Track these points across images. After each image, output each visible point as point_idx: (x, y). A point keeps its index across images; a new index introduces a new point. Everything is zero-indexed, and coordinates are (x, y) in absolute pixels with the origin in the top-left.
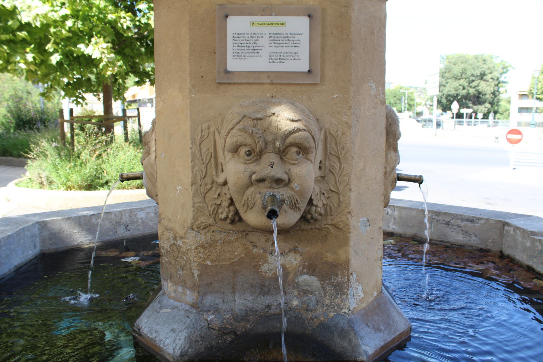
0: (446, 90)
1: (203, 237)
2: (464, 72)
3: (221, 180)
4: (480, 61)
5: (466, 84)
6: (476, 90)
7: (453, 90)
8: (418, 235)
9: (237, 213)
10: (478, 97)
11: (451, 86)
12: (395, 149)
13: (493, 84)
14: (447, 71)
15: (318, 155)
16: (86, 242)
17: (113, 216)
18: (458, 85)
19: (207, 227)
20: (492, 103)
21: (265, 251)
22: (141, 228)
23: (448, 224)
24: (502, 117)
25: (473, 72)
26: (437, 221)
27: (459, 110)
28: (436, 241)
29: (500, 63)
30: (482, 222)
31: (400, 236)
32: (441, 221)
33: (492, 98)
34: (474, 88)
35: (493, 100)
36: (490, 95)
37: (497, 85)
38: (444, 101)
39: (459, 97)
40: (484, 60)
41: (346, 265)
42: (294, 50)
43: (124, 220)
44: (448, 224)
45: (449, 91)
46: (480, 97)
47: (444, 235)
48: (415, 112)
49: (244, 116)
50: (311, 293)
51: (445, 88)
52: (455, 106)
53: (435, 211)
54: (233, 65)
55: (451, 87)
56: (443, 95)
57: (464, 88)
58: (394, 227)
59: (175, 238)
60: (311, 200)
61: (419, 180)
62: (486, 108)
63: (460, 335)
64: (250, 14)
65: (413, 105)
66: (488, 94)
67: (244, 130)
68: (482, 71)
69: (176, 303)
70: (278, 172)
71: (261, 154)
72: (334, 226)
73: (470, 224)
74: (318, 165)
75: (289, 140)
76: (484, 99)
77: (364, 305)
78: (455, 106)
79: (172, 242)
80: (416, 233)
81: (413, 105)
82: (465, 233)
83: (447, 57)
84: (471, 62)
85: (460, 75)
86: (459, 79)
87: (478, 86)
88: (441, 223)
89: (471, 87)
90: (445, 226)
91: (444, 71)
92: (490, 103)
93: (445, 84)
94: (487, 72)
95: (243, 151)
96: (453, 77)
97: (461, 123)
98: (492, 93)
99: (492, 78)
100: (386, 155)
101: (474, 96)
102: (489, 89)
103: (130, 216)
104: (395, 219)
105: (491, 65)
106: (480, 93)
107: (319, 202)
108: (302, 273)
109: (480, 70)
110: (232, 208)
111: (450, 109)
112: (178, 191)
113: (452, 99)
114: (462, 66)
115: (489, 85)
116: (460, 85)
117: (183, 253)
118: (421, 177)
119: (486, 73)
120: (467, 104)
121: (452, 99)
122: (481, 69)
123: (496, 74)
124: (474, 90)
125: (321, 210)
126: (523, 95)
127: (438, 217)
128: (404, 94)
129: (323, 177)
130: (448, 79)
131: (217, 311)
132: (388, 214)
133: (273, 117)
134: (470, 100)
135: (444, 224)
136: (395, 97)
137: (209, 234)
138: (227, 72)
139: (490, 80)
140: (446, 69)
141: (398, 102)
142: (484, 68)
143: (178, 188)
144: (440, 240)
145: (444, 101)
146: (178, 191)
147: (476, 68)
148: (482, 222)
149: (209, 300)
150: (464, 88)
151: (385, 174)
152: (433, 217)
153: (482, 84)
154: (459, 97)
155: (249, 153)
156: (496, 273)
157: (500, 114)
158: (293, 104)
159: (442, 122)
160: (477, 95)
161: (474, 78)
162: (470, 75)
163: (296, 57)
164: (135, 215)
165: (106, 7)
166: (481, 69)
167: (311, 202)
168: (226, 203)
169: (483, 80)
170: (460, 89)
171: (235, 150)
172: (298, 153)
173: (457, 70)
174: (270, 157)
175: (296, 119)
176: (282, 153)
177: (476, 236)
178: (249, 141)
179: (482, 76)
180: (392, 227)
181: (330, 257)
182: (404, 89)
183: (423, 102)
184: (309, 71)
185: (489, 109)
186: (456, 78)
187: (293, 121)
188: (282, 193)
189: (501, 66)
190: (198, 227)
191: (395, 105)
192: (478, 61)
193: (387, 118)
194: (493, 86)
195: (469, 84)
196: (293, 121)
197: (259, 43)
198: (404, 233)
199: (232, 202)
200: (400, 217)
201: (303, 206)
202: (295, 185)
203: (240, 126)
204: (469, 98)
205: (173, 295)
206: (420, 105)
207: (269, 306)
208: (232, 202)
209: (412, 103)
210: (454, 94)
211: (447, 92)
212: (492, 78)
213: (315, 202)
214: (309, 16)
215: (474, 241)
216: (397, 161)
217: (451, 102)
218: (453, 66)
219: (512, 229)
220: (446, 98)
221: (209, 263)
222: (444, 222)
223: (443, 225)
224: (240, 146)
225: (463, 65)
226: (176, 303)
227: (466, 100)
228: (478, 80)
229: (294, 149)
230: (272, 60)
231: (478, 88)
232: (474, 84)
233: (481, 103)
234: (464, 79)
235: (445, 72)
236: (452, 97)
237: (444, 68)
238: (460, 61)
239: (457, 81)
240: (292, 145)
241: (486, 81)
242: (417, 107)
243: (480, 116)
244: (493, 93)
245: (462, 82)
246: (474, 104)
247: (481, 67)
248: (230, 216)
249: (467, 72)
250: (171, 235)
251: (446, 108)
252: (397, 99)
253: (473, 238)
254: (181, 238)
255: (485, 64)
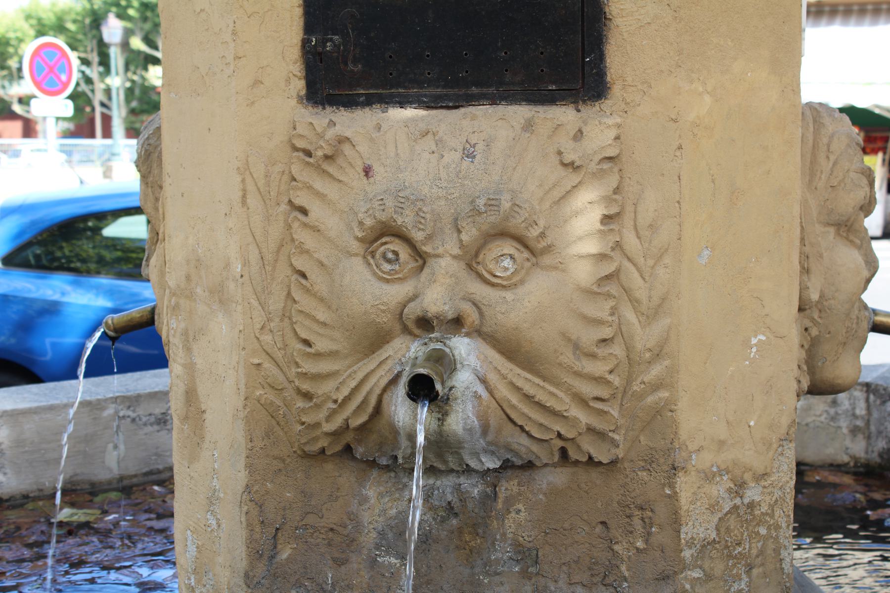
8: (79, 478)
26: (134, 420)
28: (135, 476)
32: (144, 419)
47: (156, 454)
53: (124, 397)
80: (76, 475)
88: (145, 425)
90: (156, 427)
112: (754, 350)
127: (134, 411)
135: (152, 424)
143: (754, 341)
144: (144, 471)
146: (754, 350)
152: (121, 414)
156: (77, 542)
175: (85, 160)
198: (35, 487)
200: (19, 443)
222: (153, 419)
223: (149, 429)
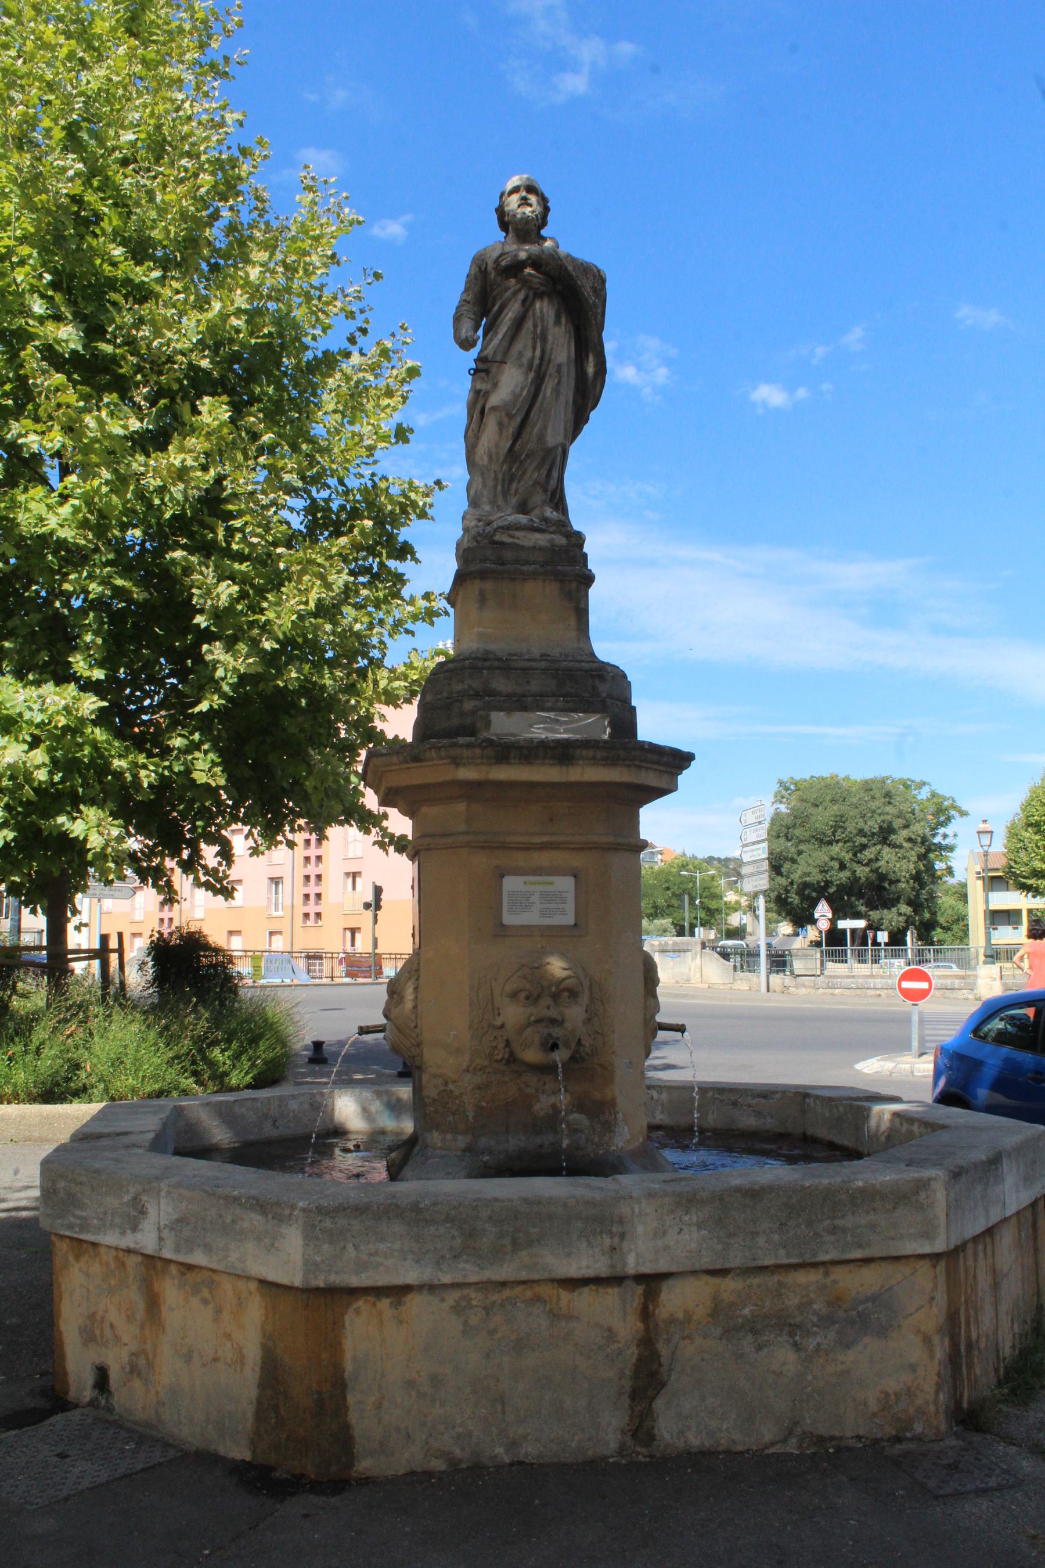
0: (799, 872)
1: (479, 1079)
2: (839, 823)
3: (498, 1023)
4: (878, 795)
5: (847, 857)
6: (871, 871)
7: (815, 871)
9: (512, 1053)
10: (880, 889)
11: (810, 862)
12: (654, 995)
13: (913, 856)
14: (799, 822)
15: (584, 999)
16: (226, 1141)
17: (259, 1104)
18: (827, 859)
19: (482, 1069)
20: (915, 904)
21: (537, 1090)
22: (292, 1125)
23: (735, 1104)
24: (947, 936)
25: (861, 825)
27: (833, 922)
29: (928, 800)
30: (778, 1096)
31: (672, 1128)
33: (913, 889)
34: (867, 865)
35: (917, 896)
36: (908, 882)
37: (922, 857)
38: (794, 899)
39: (831, 890)
40: (888, 795)
41: (612, 1103)
42: (561, 906)
43: (271, 1112)
44: (735, 1104)
45: (808, 874)
46: (884, 888)
48: (724, 927)
49: (523, 966)
50: (581, 1131)
51: (795, 866)
52: (823, 911)
54: (508, 919)
55: (809, 865)
56: (792, 883)
57: (842, 867)
58: (661, 1116)
59: (446, 1084)
60: (579, 1040)
61: (681, 1029)
62: (900, 914)
63: (450, 840)
64: (523, 874)
65: (718, 911)
66: (903, 880)
67: (524, 977)
68: (883, 821)
69: (443, 1153)
70: (553, 1013)
71: (539, 997)
72: (602, 1066)
73: (763, 1101)
74: (584, 1008)
75: (561, 987)
76: (894, 893)
77: (631, 1147)
78: (823, 911)
79: (442, 1088)
81: (718, 911)
82: (759, 1114)
83: (796, 784)
84: (854, 800)
85: (829, 832)
86: (830, 843)
87: (877, 860)
89: (859, 862)
91: (789, 821)
92: (910, 903)
93: (795, 857)
94: (898, 823)
95: (522, 995)
96: (813, 837)
97: (840, 958)
98: (913, 877)
99: (910, 840)
100: (646, 1002)
101: (870, 884)
102: (904, 867)
103: (280, 1106)
104: (663, 1105)
105: (905, 807)
106: (882, 877)
107: (587, 1042)
108: (572, 1112)
109: (879, 819)
110: (507, 1050)
111: (813, 921)
113: (814, 894)
114: (835, 809)
115: (904, 858)
116: (832, 859)
117: (456, 1098)
118: (683, 1025)
119: (895, 826)
120: (852, 906)
121: (814, 894)
122: (882, 817)
123: (918, 829)
124: (867, 869)
125: (588, 1050)
126: (992, 878)
128: (692, 880)
129: (589, 1020)
130: (801, 841)
131: (490, 1153)
132: (652, 1098)
133: (549, 967)
134: (860, 896)
136: (668, 889)
137: (485, 1076)
138: (502, 925)
139: (906, 845)
140: (795, 817)
141: (675, 902)
142: (888, 814)
145: (794, 899)
147: (869, 815)
148: (778, 1096)
149: (483, 1142)
150: (842, 867)
151: (645, 1020)
153: (887, 853)
154: (831, 890)
155: (527, 998)
157: (943, 928)
158: (563, 955)
159: (790, 955)
160: (876, 883)
161: (864, 840)
162: (854, 832)
163: (563, 913)
164: (286, 1106)
165: (108, 742)
166: (882, 817)
167: (579, 1043)
168: (502, 1045)
169: (889, 845)
170: (832, 868)
171: (514, 995)
172: (569, 997)
173: (822, 819)
174: (547, 1001)
176: (555, 997)
177: (772, 1117)
178: (528, 986)
179: (885, 834)
180: (660, 1118)
181: (597, 1095)
182: (691, 867)
183: (744, 901)
184: (575, 925)
185: (909, 917)
186: (824, 841)
187: (565, 969)
188: (556, 1032)
189: (932, 809)
190: (475, 1069)
191: (667, 912)
192: (873, 798)
193: (645, 964)
194: (914, 858)
195: (855, 855)
196: (565, 969)
197: (531, 900)
199: (508, 1044)
201: (573, 1045)
202: (568, 1025)
203: (519, 974)
204: (856, 890)
205: (439, 1145)
206: (736, 911)
207: (541, 1146)
208: (508, 1044)
209: (713, 905)
210: (818, 882)
211: (800, 877)
212: (910, 840)
213: (583, 1042)
214: (575, 876)
215: (770, 1124)
216: (657, 1008)
217: (814, 904)
218: (813, 810)
219: (812, 1100)
220: (800, 892)
221: (484, 1104)
224: (521, 990)
225: (835, 807)
226: (443, 1153)
227: (849, 896)
228: (875, 845)
229: (566, 994)
230: (543, 914)
231: (875, 865)
232: (868, 854)
233: (889, 903)
234: (840, 844)
235: (794, 826)
236: (815, 890)
237: (788, 815)
238: (829, 798)
239: (824, 849)
240: (564, 990)
241: (894, 846)
242: (727, 914)
243: (883, 937)
244: (917, 877)
245: (836, 849)
246: (872, 906)
247: (879, 811)
248: (506, 1056)
249: (847, 824)
250: (440, 1081)
251: (802, 919)
252: (673, 893)
253: (769, 1120)
254: (454, 1082)
255: (889, 803)
